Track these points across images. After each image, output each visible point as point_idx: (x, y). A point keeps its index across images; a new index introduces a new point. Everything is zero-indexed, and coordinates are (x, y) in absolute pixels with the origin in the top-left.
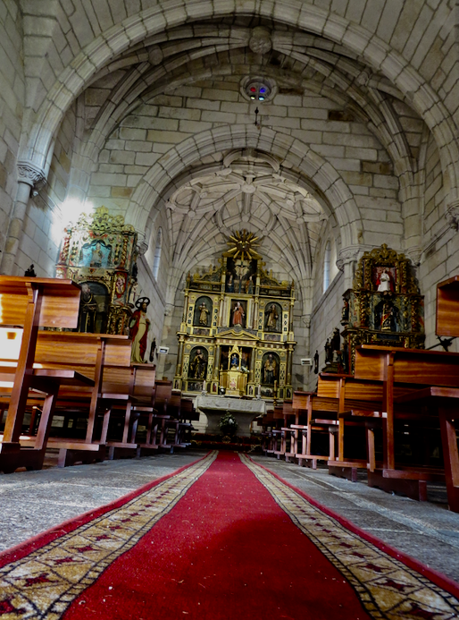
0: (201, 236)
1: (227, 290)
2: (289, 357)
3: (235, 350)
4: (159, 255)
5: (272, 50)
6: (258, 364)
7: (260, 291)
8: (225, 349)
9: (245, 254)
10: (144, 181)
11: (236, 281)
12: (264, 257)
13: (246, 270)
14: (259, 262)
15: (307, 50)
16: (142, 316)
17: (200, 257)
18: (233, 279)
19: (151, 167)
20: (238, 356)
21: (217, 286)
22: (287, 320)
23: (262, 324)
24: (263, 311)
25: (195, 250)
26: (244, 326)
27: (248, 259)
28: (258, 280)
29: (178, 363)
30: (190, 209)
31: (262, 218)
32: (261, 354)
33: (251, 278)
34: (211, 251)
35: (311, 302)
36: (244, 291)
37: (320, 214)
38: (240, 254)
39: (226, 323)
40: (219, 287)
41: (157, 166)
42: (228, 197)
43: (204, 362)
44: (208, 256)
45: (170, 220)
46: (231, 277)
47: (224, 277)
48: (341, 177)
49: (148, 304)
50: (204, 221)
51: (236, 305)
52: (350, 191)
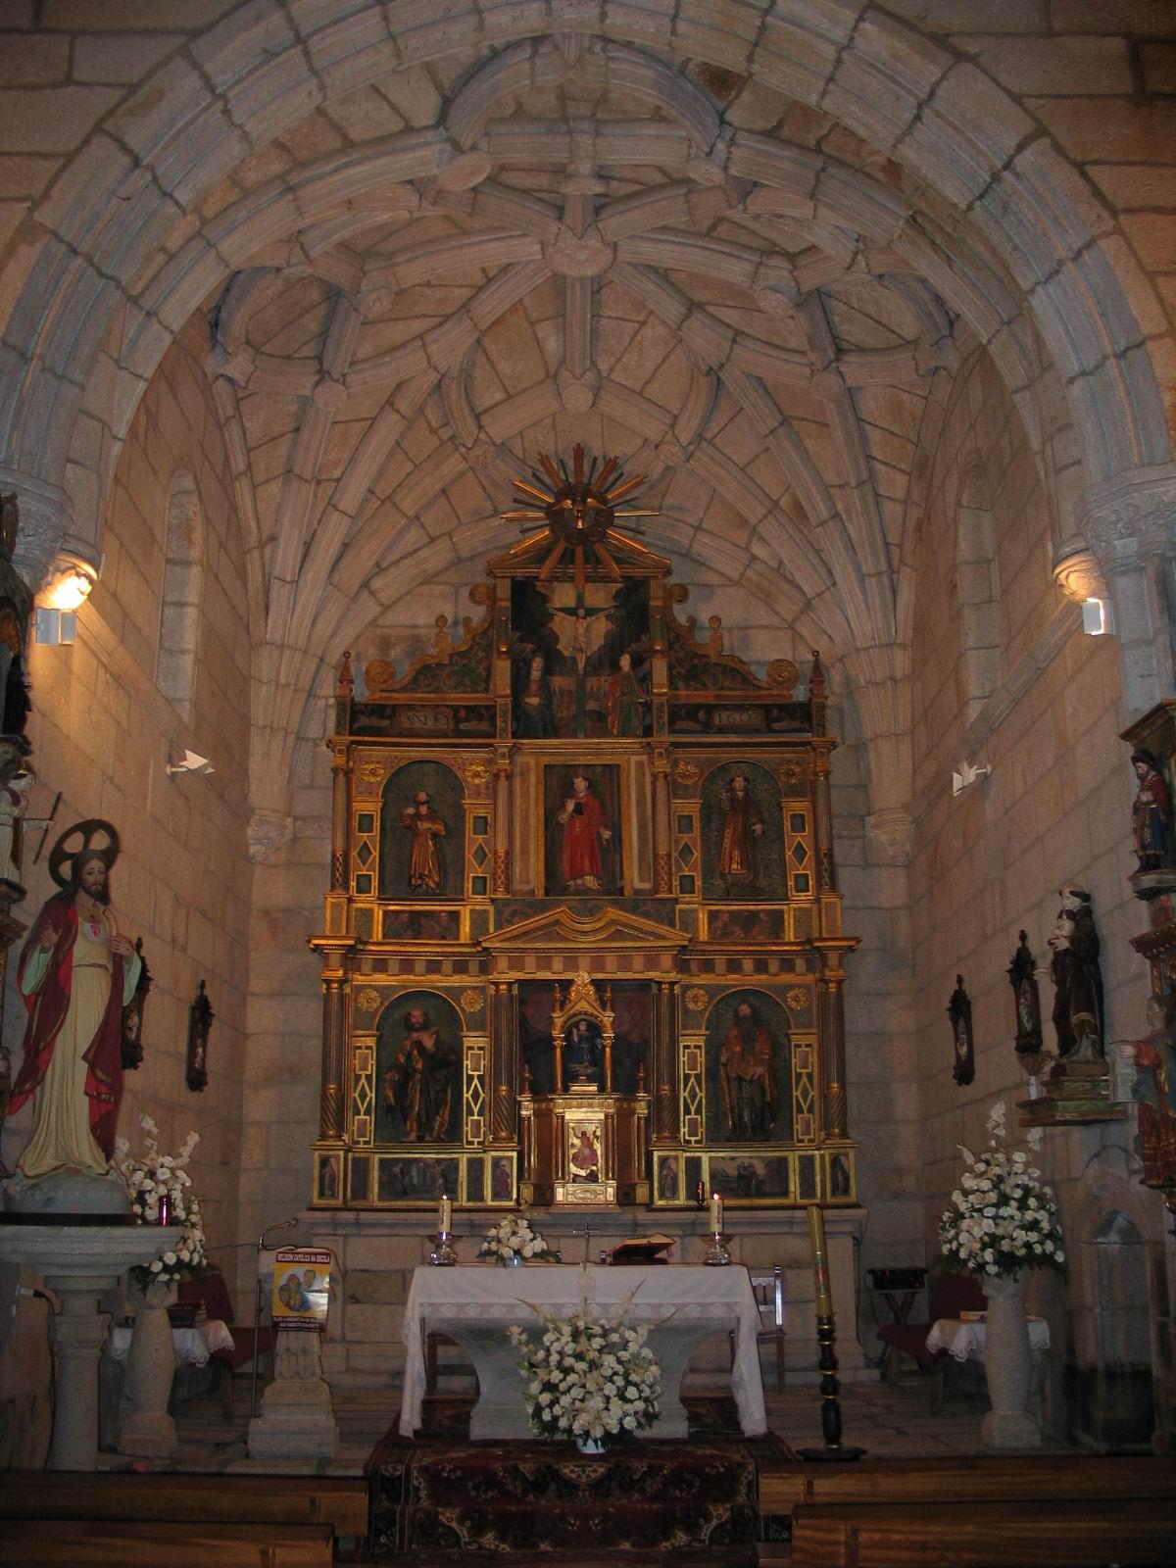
0: (385, 490)
1: (526, 725)
2: (831, 1012)
3: (583, 1000)
4: (193, 597)
5: (555, 275)
6: (691, 1049)
7: (674, 717)
8: (538, 995)
9: (592, 558)
10: (41, 228)
11: (558, 682)
12: (675, 562)
13: (601, 627)
14: (655, 590)
15: (357, 1219)
16: (84, 927)
17: (388, 585)
18: (548, 671)
19: (70, 157)
20: (595, 1029)
21: (474, 712)
22: (803, 838)
23: (693, 868)
24: (691, 807)
25: (364, 559)
26: (613, 889)
27: (606, 579)
28: (659, 669)
29: (325, 1081)
30: (322, 374)
31: (654, 390)
32: (699, 1002)
33: (625, 662)
34: (437, 557)
35: (905, 748)
36: (599, 724)
37: (914, 343)
38: (568, 558)
39: (531, 873)
40: (484, 713)
41: (101, 146)
42: (490, 307)
43: (446, 1063)
44: (429, 580)
45: (233, 432)
46: (537, 664)
47: (503, 669)
48: (1041, 131)
49: (110, 856)
50: (390, 427)
51: (568, 790)
52: (1098, 193)
